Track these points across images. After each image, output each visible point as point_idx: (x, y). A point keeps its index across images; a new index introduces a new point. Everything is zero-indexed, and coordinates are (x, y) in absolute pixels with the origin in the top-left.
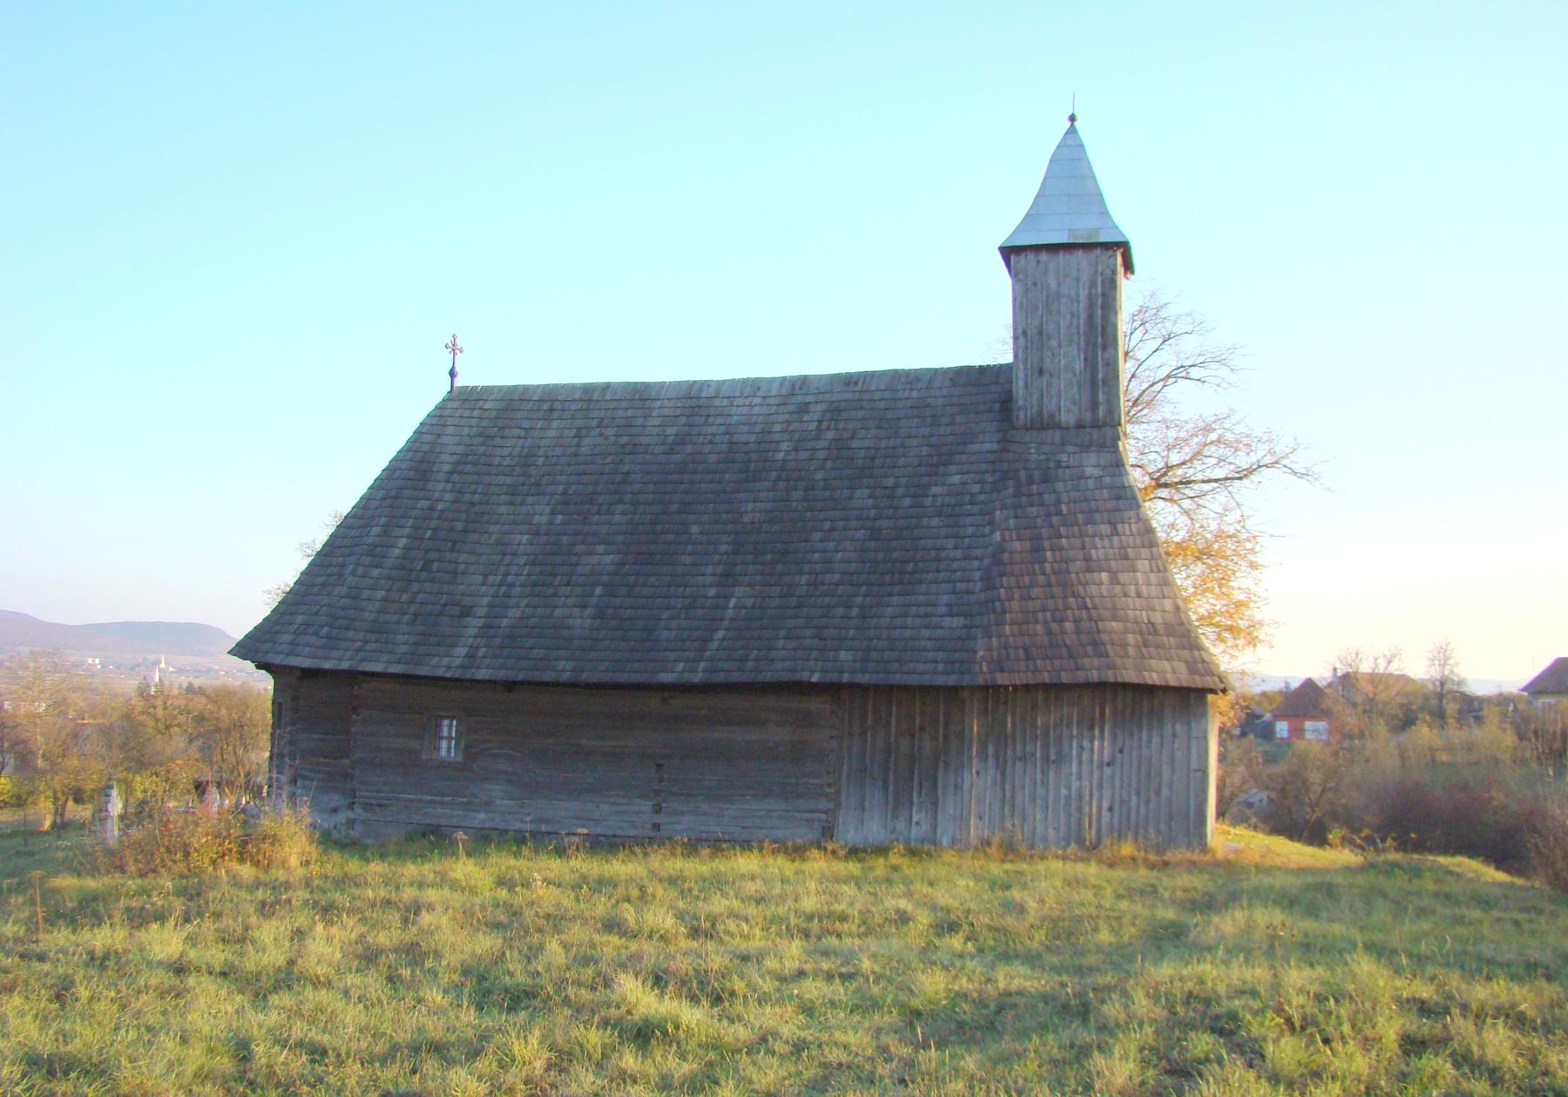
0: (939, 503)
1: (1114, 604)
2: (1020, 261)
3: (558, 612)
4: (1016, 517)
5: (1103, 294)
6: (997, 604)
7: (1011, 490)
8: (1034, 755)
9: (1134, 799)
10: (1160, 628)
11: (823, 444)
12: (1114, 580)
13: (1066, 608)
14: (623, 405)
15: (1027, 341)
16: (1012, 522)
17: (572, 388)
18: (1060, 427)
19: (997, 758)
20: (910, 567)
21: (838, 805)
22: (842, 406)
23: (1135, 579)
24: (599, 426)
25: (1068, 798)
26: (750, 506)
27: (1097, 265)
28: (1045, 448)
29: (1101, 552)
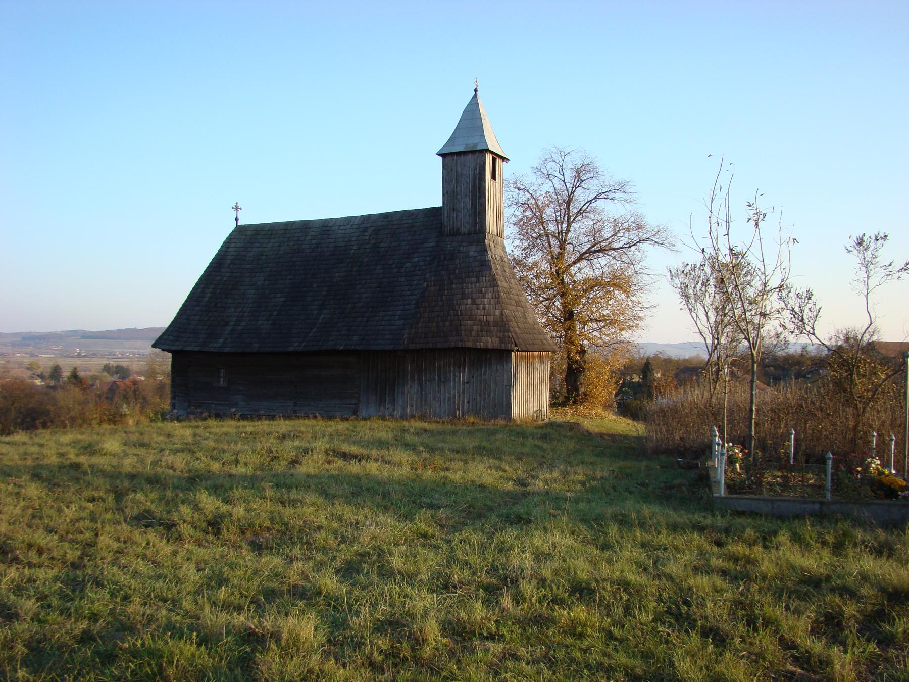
0: (407, 270)
1: (471, 313)
2: (449, 158)
3: (260, 323)
4: (435, 276)
5: (479, 173)
6: (419, 314)
7: (436, 264)
8: (434, 379)
9: (479, 397)
10: (491, 323)
11: (370, 245)
12: (473, 302)
13: (449, 315)
16: (433, 278)
17: (281, 223)
18: (462, 235)
20: (390, 299)
23: (484, 302)
24: (288, 241)
25: (449, 398)
26: (337, 274)
28: (454, 244)
29: (470, 290)
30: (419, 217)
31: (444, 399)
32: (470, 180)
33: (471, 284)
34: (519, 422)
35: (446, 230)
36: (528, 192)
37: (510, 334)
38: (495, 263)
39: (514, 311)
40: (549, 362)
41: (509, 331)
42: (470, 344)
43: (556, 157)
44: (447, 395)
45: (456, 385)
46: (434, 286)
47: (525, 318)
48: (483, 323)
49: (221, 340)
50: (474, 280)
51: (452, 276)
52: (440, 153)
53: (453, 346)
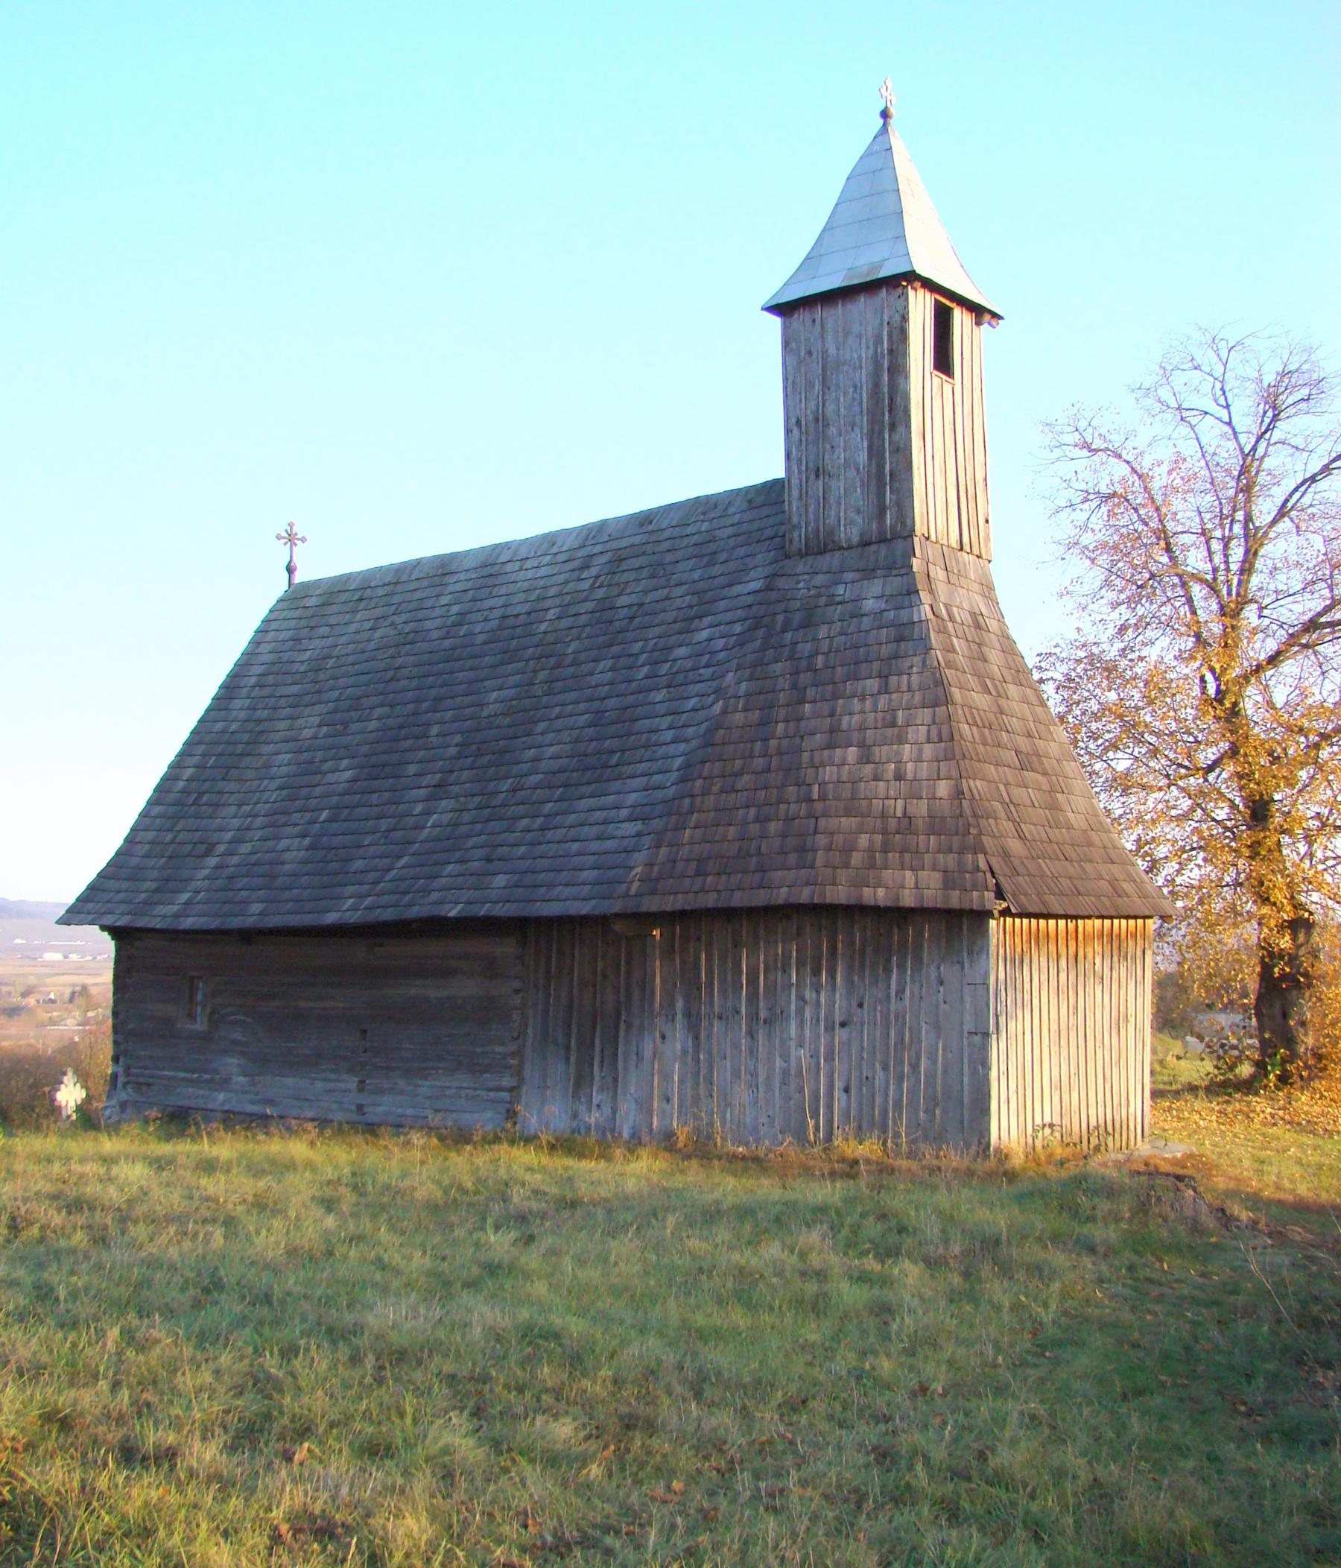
2: (802, 317)
5: (891, 351)
7: (757, 644)
9: (880, 1074)
10: (920, 823)
11: (589, 606)
12: (865, 758)
14: (425, 583)
15: (801, 433)
18: (841, 548)
19: (688, 1015)
20: (615, 759)
21: (521, 1081)
22: (624, 554)
25: (785, 1073)
27: (882, 313)
28: (819, 580)
29: (856, 718)
30: (731, 510)
31: (769, 1078)
32: (863, 376)
33: (863, 698)
34: (1017, 1161)
35: (796, 535)
36: (1119, 456)
37: (981, 857)
38: (942, 631)
39: (1007, 784)
40: (1148, 953)
41: (978, 848)
42: (839, 894)
43: (1207, 358)
44: (779, 1063)
45: (807, 1032)
46: (745, 710)
47: (1054, 807)
48: (892, 823)
49: (185, 897)
50: (872, 685)
51: (804, 678)
52: (775, 302)
53: (781, 901)
